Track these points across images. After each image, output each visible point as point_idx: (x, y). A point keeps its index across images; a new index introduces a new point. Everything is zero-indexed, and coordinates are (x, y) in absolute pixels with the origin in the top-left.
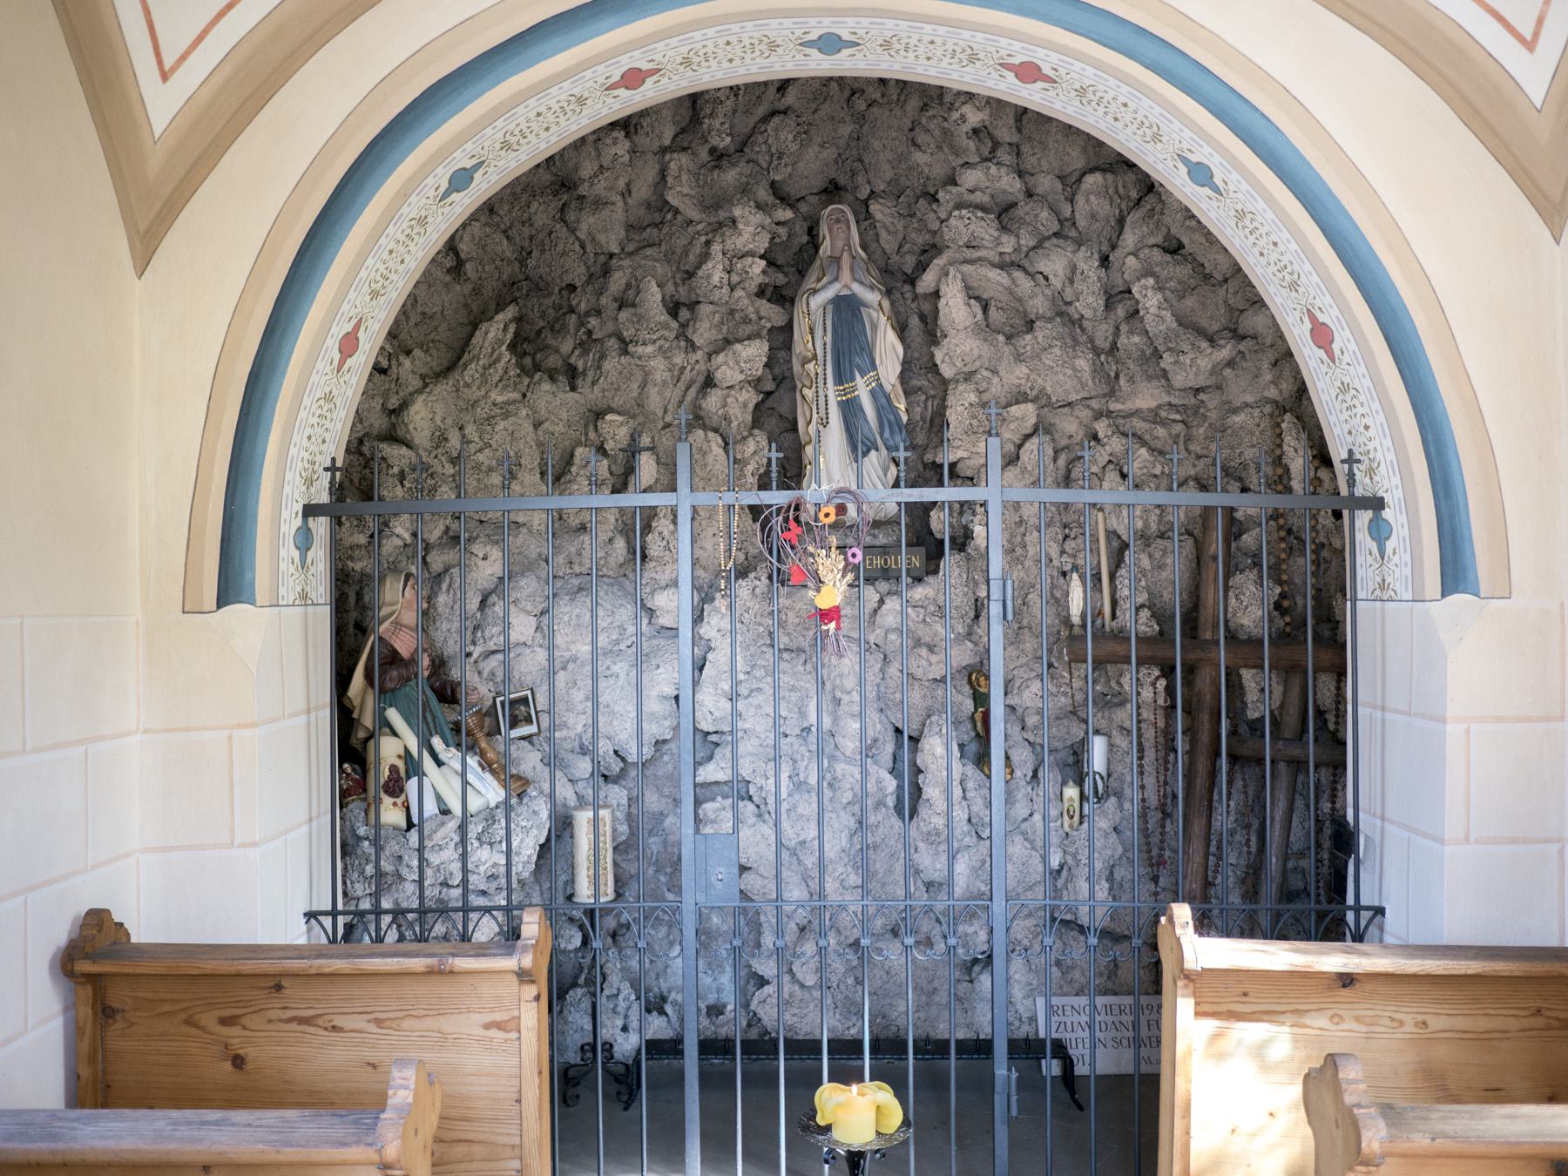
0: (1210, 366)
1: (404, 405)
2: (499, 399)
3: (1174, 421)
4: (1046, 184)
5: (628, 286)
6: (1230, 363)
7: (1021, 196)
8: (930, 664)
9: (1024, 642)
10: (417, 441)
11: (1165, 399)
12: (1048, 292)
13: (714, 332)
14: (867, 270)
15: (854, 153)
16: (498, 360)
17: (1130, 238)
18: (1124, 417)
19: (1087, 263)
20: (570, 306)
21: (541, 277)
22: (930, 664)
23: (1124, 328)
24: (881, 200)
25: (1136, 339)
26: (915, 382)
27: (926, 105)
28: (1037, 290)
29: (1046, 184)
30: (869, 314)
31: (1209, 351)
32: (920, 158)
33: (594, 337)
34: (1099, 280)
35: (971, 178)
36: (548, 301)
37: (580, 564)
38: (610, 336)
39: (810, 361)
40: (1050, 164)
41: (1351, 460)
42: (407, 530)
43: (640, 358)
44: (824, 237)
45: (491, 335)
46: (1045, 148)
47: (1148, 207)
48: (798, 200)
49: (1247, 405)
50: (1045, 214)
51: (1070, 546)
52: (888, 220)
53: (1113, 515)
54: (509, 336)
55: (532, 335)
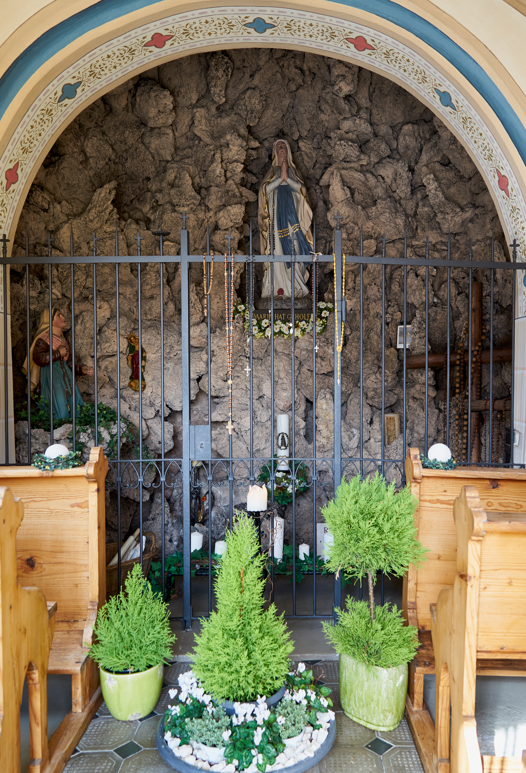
0: (461, 221)
1: (58, 229)
2: (108, 230)
3: (443, 250)
4: (384, 129)
5: (176, 177)
6: (471, 221)
7: (371, 136)
8: (322, 366)
9: (368, 356)
10: (65, 248)
11: (440, 239)
12: (384, 185)
13: (218, 201)
14: (296, 173)
15: (291, 115)
16: (106, 208)
17: (424, 158)
18: (419, 248)
19: (402, 168)
20: (148, 188)
21: (132, 173)
22: (322, 366)
23: (420, 204)
24: (305, 141)
25: (426, 209)
26: (321, 234)
27: (325, 86)
28: (378, 184)
29: (384, 129)
30: (296, 195)
31: (461, 213)
32: (323, 117)
33: (159, 203)
34: (408, 178)
35: (346, 125)
36: (136, 186)
37: (150, 315)
38: (167, 203)
39: (266, 218)
40: (386, 119)
41: (515, 245)
42: (59, 291)
43: (181, 213)
44: (275, 156)
45: (102, 195)
46: (384, 111)
47: (434, 141)
48: (264, 140)
49: (478, 241)
50: (383, 146)
51: (390, 310)
52: (308, 151)
53: (412, 295)
54: (112, 197)
55: (129, 203)
